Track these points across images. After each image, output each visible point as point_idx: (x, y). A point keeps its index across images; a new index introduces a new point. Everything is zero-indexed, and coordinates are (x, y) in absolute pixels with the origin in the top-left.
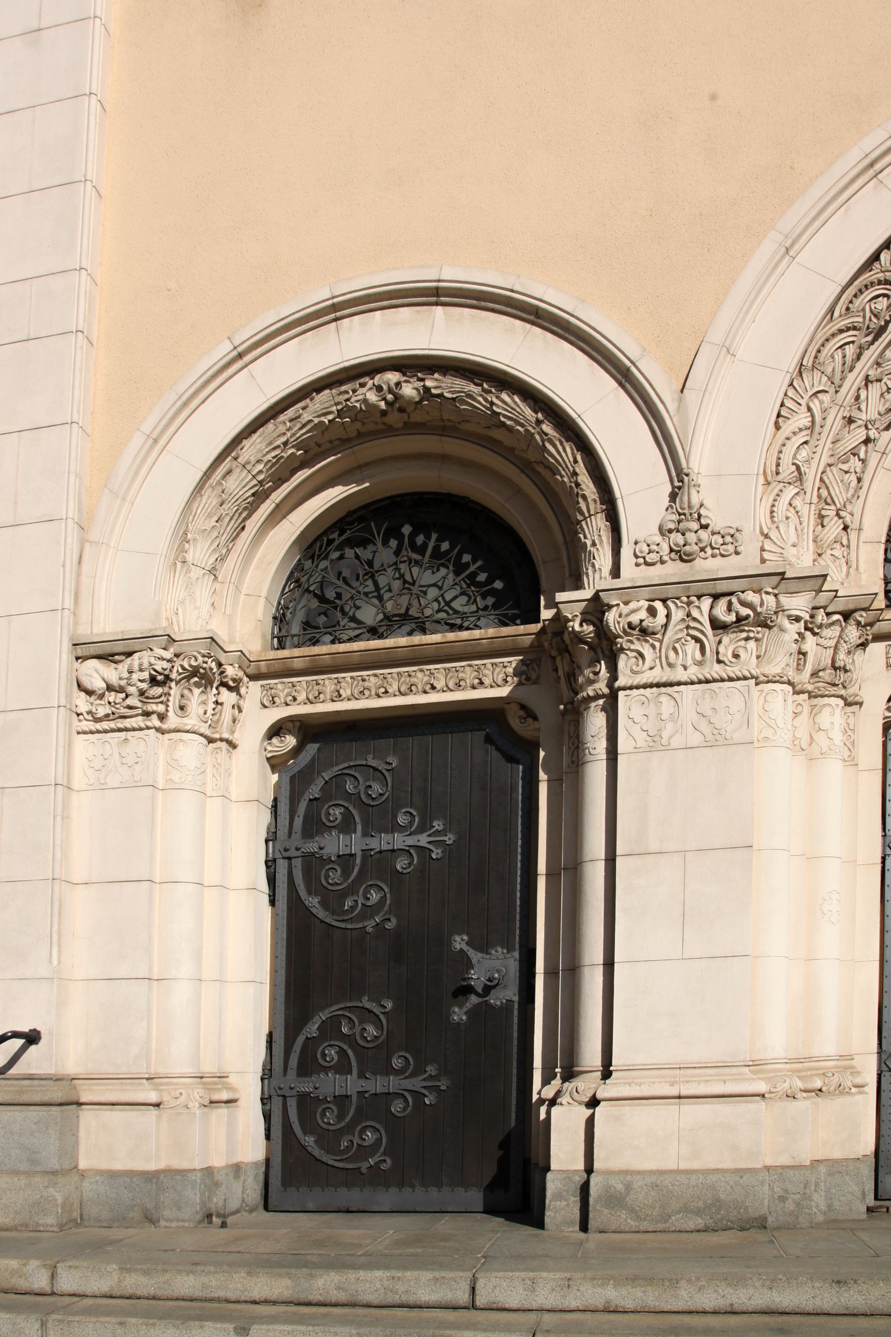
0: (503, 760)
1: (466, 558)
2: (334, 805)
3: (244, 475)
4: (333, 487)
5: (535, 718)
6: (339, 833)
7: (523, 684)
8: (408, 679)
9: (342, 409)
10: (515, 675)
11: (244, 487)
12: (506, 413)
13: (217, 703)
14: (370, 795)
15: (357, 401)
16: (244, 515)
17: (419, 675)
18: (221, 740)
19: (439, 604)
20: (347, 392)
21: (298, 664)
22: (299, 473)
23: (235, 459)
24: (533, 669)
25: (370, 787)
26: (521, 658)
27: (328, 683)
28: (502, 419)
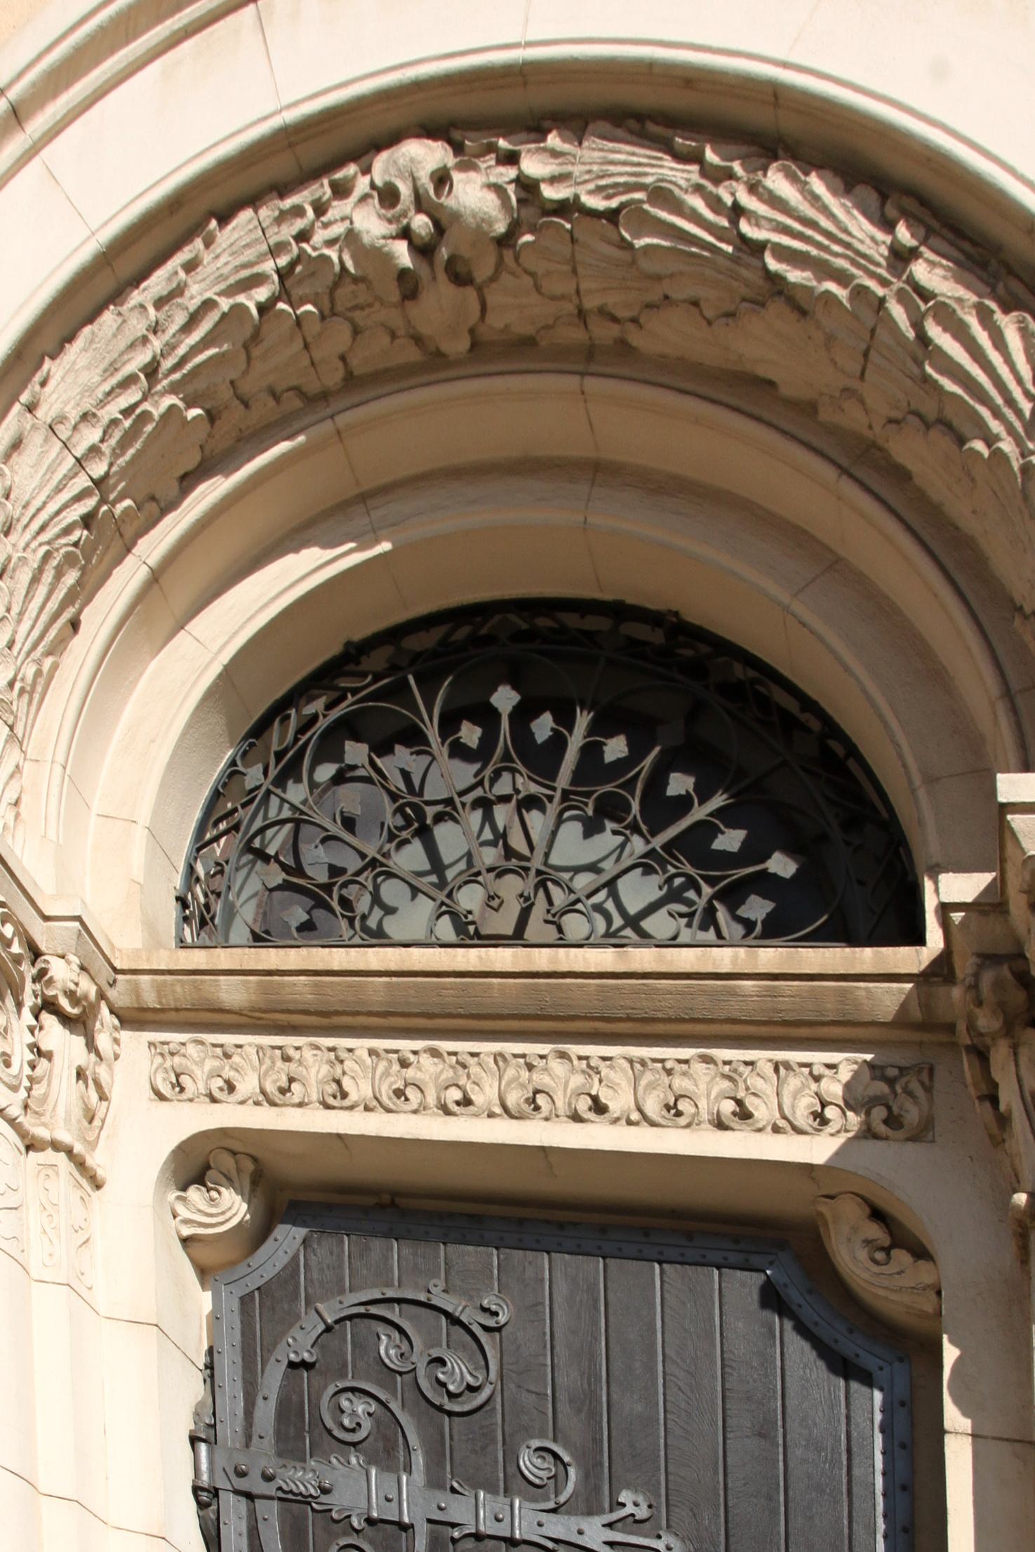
0: (821, 1364)
1: (679, 784)
2: (353, 1390)
3: (53, 454)
4: (296, 550)
5: (921, 1253)
6: (370, 1462)
7: (876, 1137)
8: (525, 1074)
9: (292, 265)
10: (851, 1102)
11: (58, 490)
12: (786, 241)
13: (36, 1049)
14: (443, 1385)
15: (330, 243)
16: (71, 577)
17: (557, 1066)
18: (56, 1146)
19: (609, 921)
20: (298, 211)
21: (232, 993)
22: (202, 488)
23: (31, 408)
24: (910, 1094)
25: (441, 1362)
26: (869, 1057)
27: (312, 1057)
28: (773, 264)
